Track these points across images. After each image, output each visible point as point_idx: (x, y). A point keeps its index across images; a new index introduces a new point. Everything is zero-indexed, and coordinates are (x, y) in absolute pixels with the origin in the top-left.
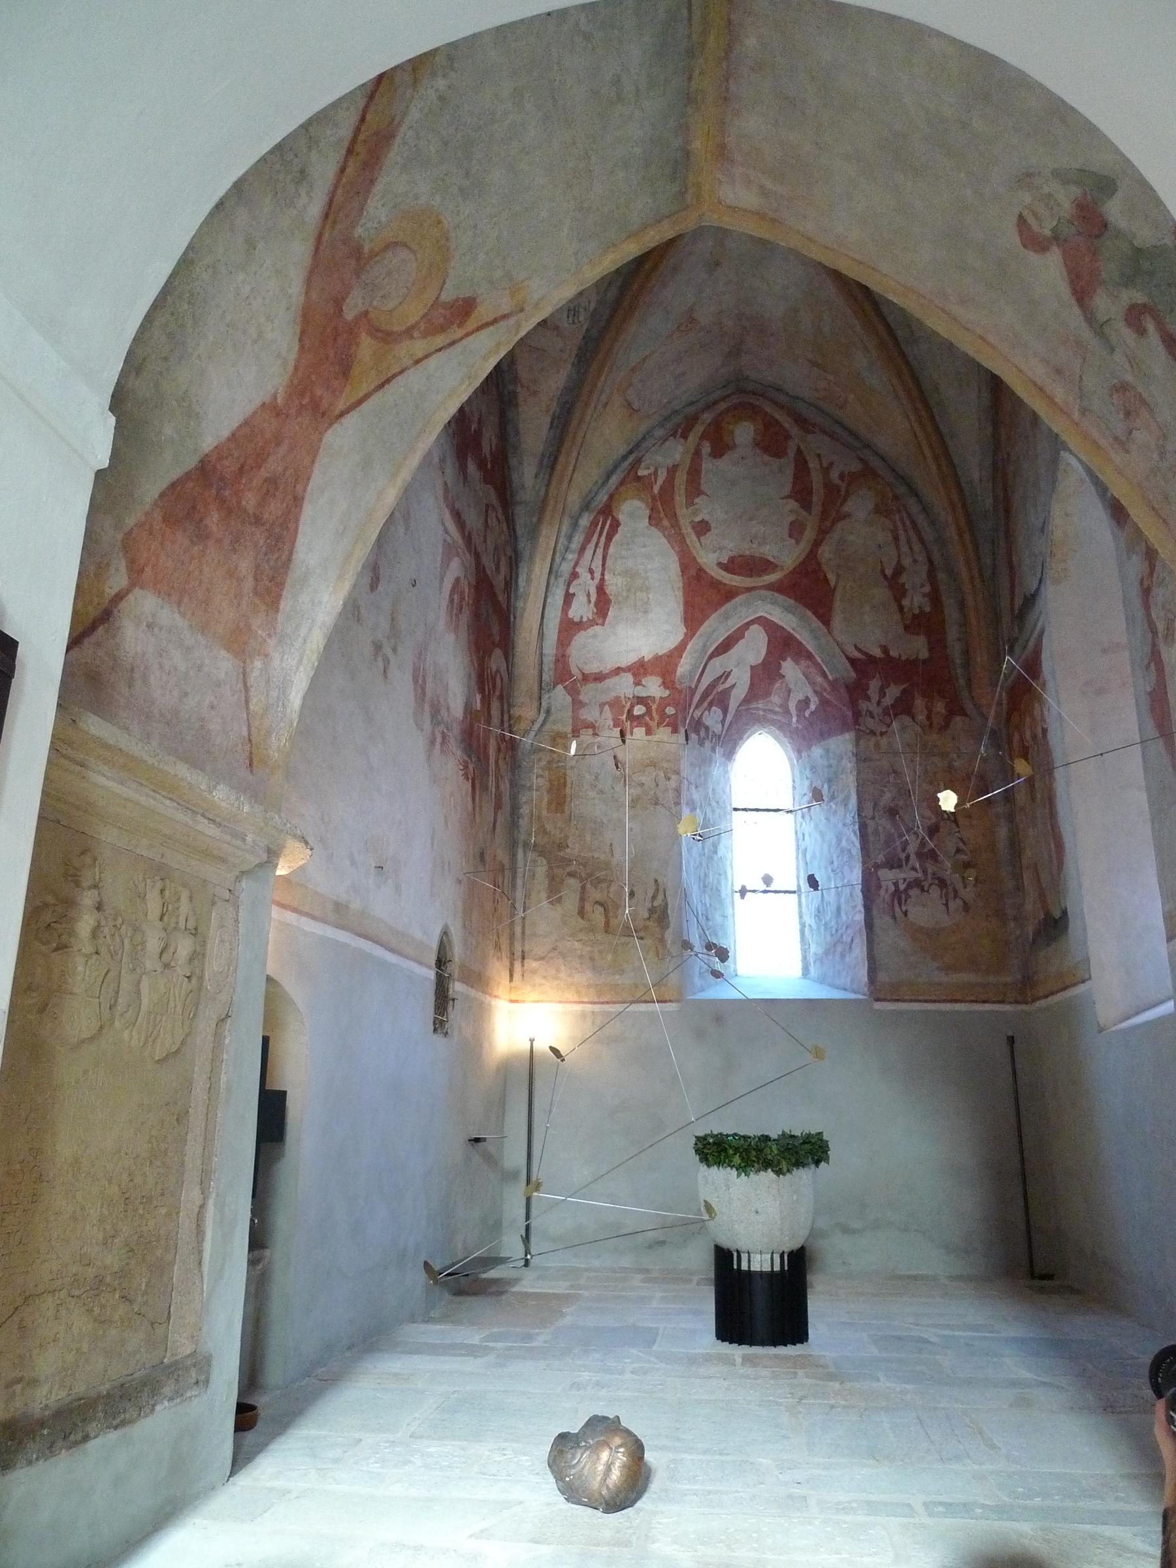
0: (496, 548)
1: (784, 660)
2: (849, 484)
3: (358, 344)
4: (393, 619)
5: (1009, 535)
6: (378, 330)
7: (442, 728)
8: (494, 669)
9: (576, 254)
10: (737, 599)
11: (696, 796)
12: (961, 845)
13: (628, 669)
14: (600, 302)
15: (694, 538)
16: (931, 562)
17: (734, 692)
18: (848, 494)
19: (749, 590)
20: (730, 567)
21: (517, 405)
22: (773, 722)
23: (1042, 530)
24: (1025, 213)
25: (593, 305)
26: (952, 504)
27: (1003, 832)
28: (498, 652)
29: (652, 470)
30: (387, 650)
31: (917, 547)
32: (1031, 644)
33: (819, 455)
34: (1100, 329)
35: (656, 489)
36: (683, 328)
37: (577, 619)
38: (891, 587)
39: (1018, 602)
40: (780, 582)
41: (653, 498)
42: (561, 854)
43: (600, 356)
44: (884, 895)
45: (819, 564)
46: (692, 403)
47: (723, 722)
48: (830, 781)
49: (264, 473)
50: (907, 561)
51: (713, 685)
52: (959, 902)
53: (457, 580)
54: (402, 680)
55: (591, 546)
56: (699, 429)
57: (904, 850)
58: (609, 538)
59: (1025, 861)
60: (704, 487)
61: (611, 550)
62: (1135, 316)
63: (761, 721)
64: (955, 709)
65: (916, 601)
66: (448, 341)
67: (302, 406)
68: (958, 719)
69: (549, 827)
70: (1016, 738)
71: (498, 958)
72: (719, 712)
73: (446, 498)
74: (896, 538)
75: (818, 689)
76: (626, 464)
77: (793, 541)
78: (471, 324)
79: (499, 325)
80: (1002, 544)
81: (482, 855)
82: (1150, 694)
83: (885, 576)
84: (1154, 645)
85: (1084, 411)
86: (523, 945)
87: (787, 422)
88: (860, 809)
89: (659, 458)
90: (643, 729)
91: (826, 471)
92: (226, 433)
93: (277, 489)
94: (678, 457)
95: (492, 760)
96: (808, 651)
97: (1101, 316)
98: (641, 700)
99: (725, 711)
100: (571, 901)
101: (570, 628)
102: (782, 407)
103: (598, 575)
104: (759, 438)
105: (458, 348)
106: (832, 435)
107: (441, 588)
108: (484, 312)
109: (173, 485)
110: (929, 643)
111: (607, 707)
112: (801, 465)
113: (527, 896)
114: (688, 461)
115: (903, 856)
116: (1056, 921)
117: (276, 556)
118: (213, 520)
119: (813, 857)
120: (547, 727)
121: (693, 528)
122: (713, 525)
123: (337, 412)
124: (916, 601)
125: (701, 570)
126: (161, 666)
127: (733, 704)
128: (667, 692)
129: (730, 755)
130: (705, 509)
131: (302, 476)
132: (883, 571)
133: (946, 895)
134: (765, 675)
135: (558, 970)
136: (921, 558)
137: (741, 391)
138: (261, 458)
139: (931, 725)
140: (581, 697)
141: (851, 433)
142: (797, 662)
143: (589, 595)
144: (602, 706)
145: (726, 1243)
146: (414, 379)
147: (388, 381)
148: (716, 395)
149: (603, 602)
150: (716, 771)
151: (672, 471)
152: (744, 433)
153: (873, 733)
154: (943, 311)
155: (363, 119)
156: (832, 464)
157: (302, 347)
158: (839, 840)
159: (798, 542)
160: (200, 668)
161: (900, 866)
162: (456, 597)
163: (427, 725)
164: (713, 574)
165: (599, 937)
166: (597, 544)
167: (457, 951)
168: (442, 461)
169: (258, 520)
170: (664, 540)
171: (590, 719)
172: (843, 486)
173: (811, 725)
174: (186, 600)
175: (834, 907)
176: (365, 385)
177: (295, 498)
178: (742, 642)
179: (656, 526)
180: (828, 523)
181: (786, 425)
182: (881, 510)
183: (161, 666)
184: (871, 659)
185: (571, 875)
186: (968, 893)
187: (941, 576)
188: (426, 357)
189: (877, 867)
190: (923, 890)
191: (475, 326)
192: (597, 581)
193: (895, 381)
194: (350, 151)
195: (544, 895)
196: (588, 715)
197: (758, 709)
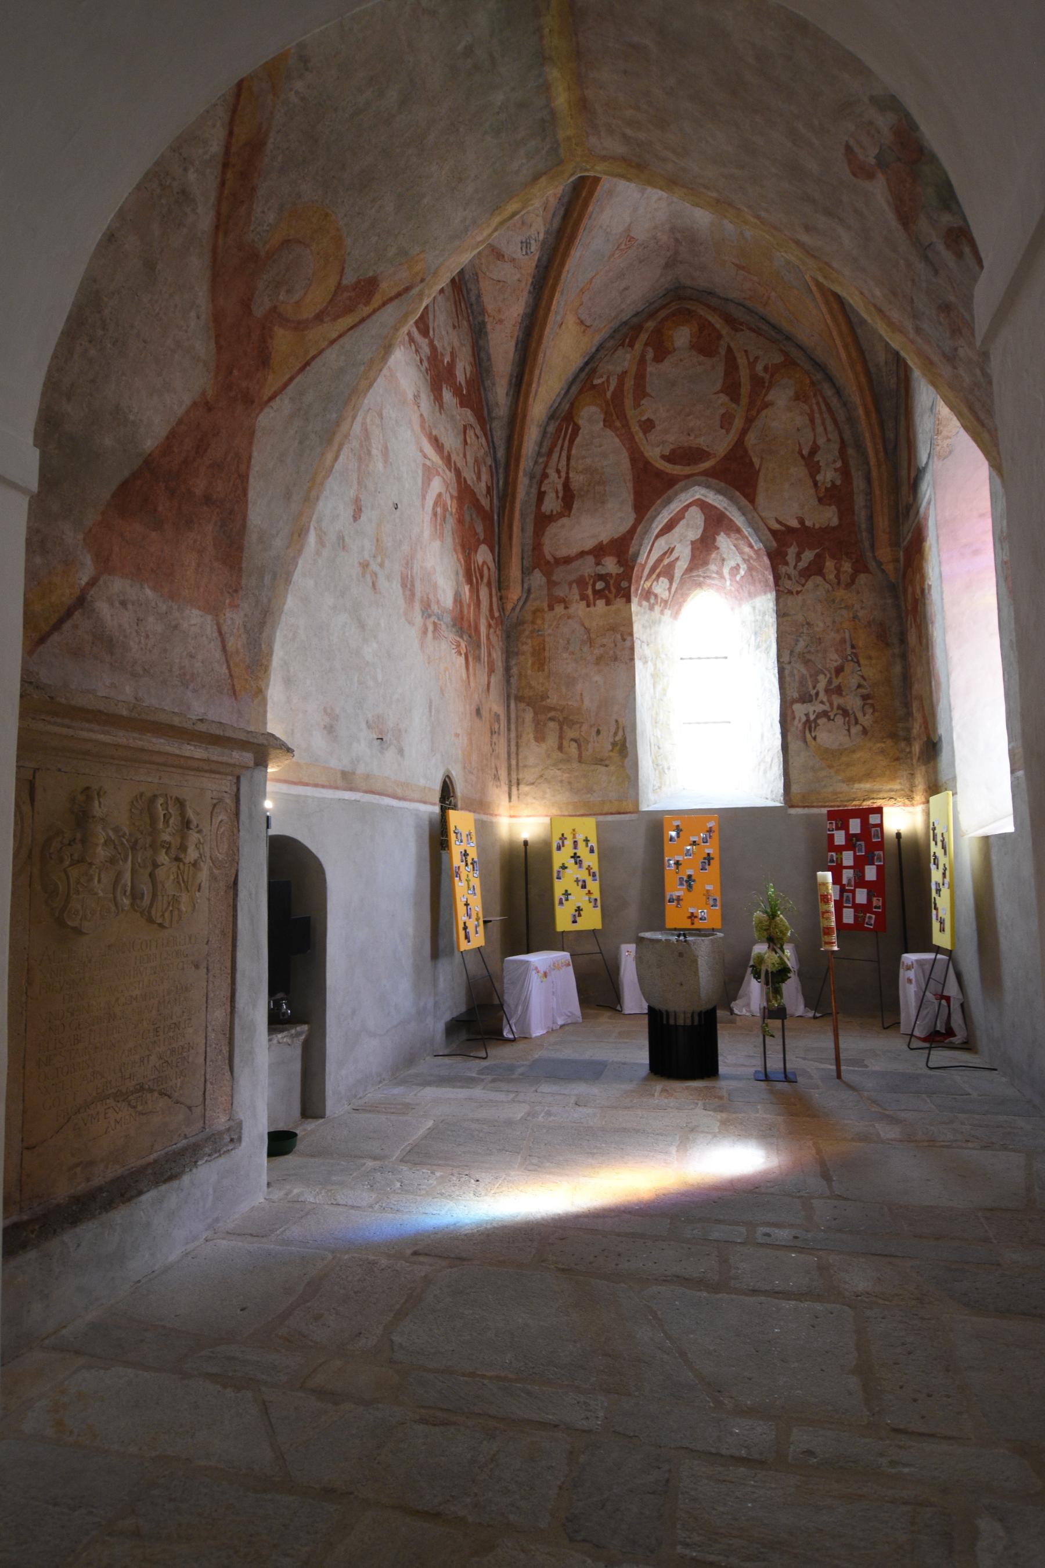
0: (476, 461)
1: (718, 534)
2: (772, 376)
4: (378, 540)
7: (433, 619)
8: (480, 563)
10: (677, 487)
12: (863, 682)
13: (590, 552)
14: (547, 232)
15: (641, 434)
17: (679, 563)
19: (688, 477)
20: (671, 458)
21: (486, 334)
24: (852, 143)
25: (541, 237)
27: (898, 669)
28: (483, 549)
29: (605, 377)
30: (374, 567)
31: (830, 427)
33: (746, 351)
34: (924, 251)
35: (609, 395)
36: (623, 247)
37: (548, 513)
38: (807, 465)
40: (713, 467)
42: (544, 703)
43: (551, 282)
44: (797, 724)
45: (746, 452)
46: (637, 314)
47: (670, 589)
50: (821, 441)
51: (660, 560)
52: (859, 728)
53: (440, 495)
54: (392, 589)
55: (557, 449)
56: (644, 337)
57: (814, 688)
58: (572, 442)
60: (648, 390)
61: (573, 452)
64: (860, 567)
65: (828, 476)
66: (357, 320)
69: (533, 683)
71: (497, 787)
72: (666, 581)
73: (423, 427)
74: (812, 420)
75: (746, 557)
76: (583, 375)
77: (724, 431)
80: (902, 418)
83: (802, 456)
86: (518, 774)
87: (718, 323)
89: (610, 367)
90: (604, 601)
91: (752, 365)
94: (626, 364)
96: (736, 526)
98: (601, 577)
99: (671, 581)
100: (552, 741)
101: (543, 521)
102: (714, 309)
103: (563, 474)
104: (695, 340)
106: (757, 331)
107: (423, 506)
108: (386, 287)
111: (574, 585)
113: (518, 737)
115: (813, 692)
120: (529, 603)
121: (640, 426)
122: (657, 422)
123: (265, 398)
125: (647, 463)
127: (678, 573)
128: (622, 569)
130: (650, 409)
133: (848, 722)
135: (545, 793)
136: (834, 436)
139: (839, 583)
140: (554, 578)
141: (774, 327)
143: (557, 492)
152: (682, 336)
153: (790, 592)
155: (231, 133)
156: (757, 358)
159: (728, 431)
161: (811, 701)
162: (439, 510)
163: (418, 619)
164: (657, 465)
165: (575, 765)
166: (562, 447)
168: (416, 397)
169: (207, 500)
170: (616, 440)
171: (562, 595)
173: (741, 586)
178: (683, 523)
179: (610, 427)
180: (754, 413)
181: (718, 326)
182: (800, 397)
184: (790, 530)
185: (552, 719)
186: (866, 720)
187: (851, 451)
189: (794, 701)
190: (829, 719)
191: (380, 302)
192: (563, 479)
194: (225, 165)
195: (531, 736)
196: (560, 592)
197: (699, 576)
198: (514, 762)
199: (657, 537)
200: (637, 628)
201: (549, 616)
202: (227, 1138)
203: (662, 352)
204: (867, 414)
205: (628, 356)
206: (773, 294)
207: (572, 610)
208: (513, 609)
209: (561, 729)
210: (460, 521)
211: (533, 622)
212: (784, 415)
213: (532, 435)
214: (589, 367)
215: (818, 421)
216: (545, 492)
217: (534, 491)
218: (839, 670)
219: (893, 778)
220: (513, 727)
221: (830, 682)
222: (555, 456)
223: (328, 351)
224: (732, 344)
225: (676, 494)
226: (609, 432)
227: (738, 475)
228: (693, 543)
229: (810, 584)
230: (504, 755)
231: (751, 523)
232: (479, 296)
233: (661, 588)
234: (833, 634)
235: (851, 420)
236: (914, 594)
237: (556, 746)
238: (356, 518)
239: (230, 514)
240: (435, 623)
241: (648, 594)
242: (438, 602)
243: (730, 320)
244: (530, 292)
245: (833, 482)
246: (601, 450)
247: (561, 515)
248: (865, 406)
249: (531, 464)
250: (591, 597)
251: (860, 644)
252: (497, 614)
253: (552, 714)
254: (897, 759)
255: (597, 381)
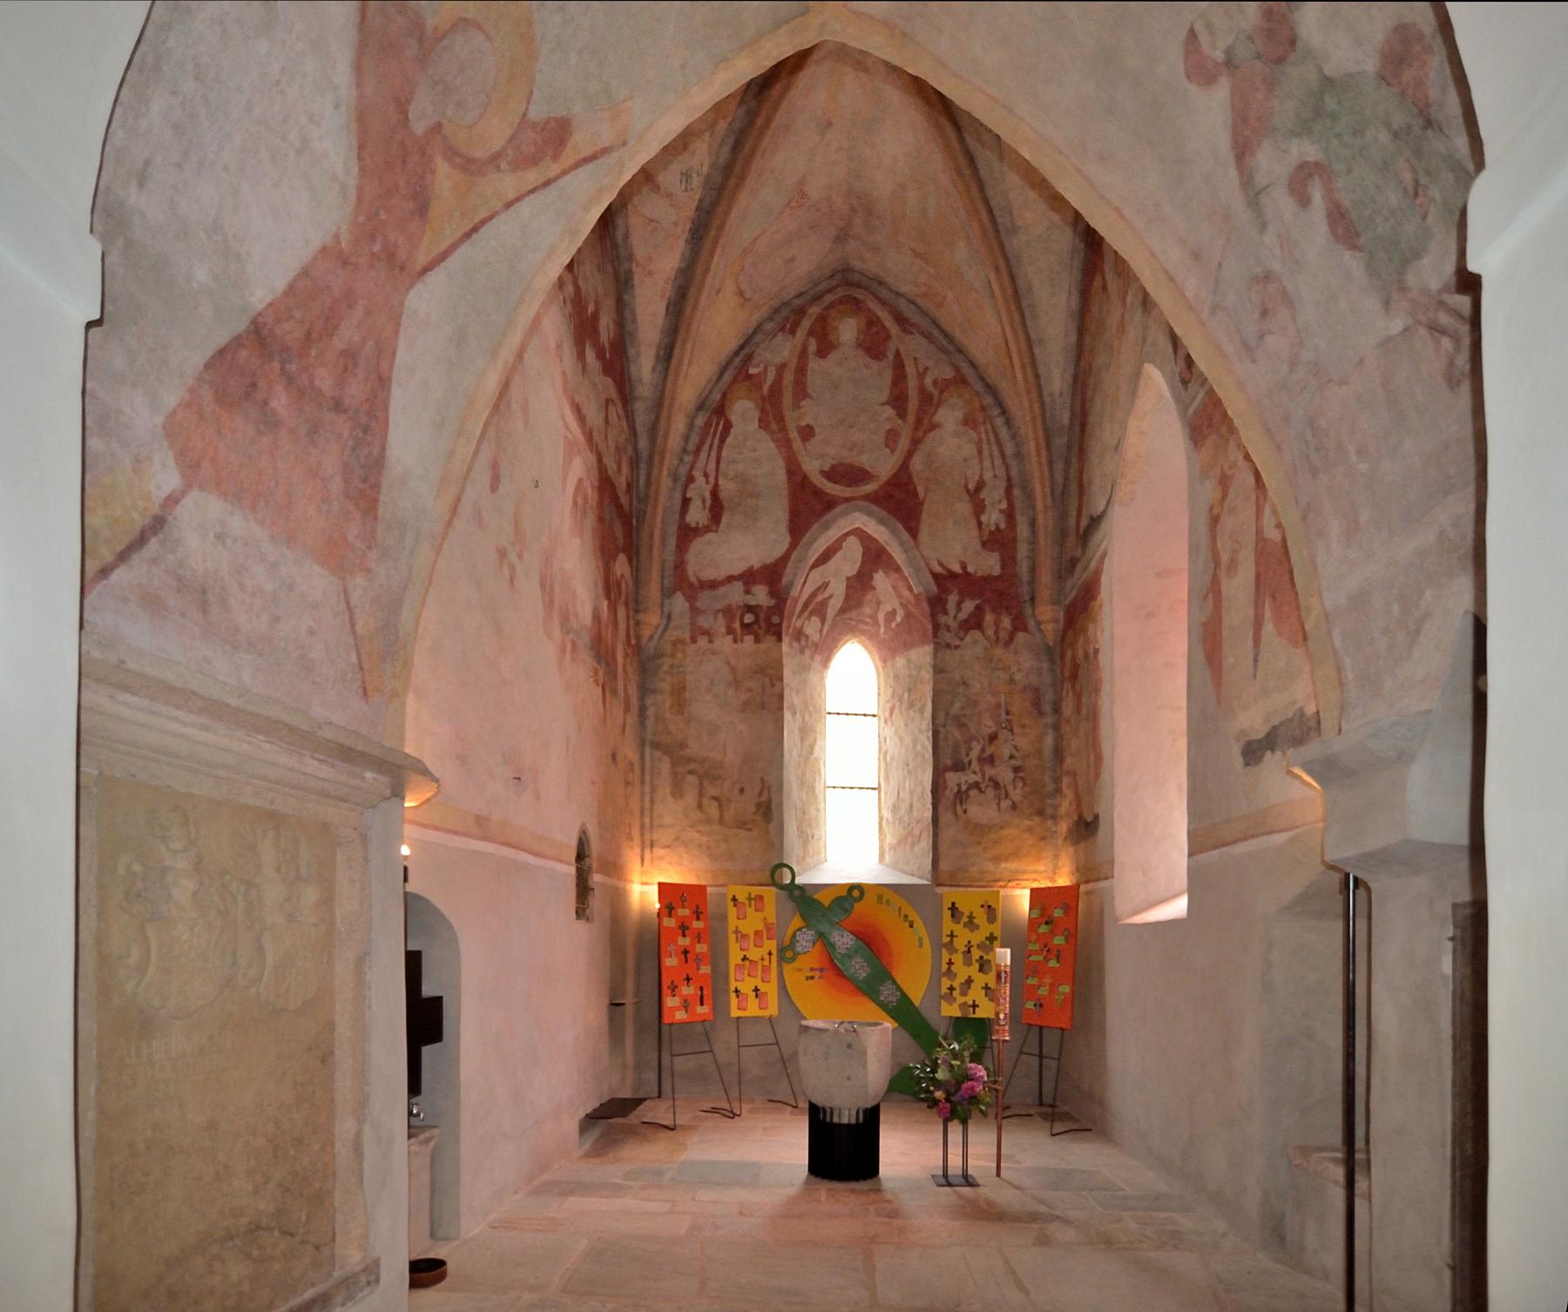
2: (942, 392)
3: (433, 172)
5: (1082, 452)
6: (456, 153)
7: (572, 636)
9: (683, 67)
11: (797, 701)
14: (713, 166)
16: (1009, 479)
17: (832, 601)
18: (940, 402)
19: (847, 500)
20: (832, 475)
22: (863, 633)
23: (1116, 448)
25: (705, 169)
26: (1033, 419)
27: (1049, 741)
28: (622, 558)
30: (513, 556)
31: (998, 462)
32: (1093, 565)
34: (1254, 196)
39: (1084, 522)
40: (875, 492)
41: (763, 399)
43: (713, 233)
45: (910, 475)
46: (801, 295)
48: (909, 690)
49: (339, 343)
50: (988, 476)
51: (813, 595)
53: (580, 481)
54: (529, 587)
55: (706, 447)
56: (806, 324)
59: (1065, 767)
60: (809, 390)
61: (724, 453)
62: (1300, 181)
63: (853, 630)
64: (1019, 625)
65: (993, 517)
66: (542, 180)
67: (373, 254)
68: (1021, 634)
69: (672, 728)
70: (1069, 654)
73: (565, 390)
74: (980, 451)
76: (737, 360)
78: (569, 156)
79: (599, 162)
81: (614, 758)
82: (1204, 624)
84: (1215, 576)
85: (1214, 309)
87: (889, 322)
88: (934, 717)
89: (768, 355)
91: (921, 376)
92: (280, 285)
93: (356, 365)
94: (786, 353)
95: (620, 668)
97: (1261, 180)
98: (750, 609)
99: (823, 621)
100: (690, 798)
101: (687, 534)
102: (884, 303)
103: (712, 480)
105: (552, 191)
106: (929, 337)
107: (563, 490)
108: (581, 142)
109: (221, 352)
110: (1003, 560)
112: (899, 366)
113: (653, 791)
114: (795, 360)
116: (1087, 824)
117: (366, 451)
118: (280, 401)
119: (892, 758)
122: (817, 430)
123: (419, 268)
124: (993, 517)
125: (805, 477)
126: (241, 586)
127: (831, 612)
128: (772, 602)
129: (826, 663)
131: (385, 351)
132: (966, 486)
134: (860, 584)
136: (1001, 472)
137: (848, 284)
138: (331, 322)
140: (698, 604)
141: (946, 335)
142: (886, 574)
144: (717, 612)
145: (819, 1101)
146: (503, 230)
147: (475, 229)
148: (821, 287)
149: (716, 509)
150: (813, 678)
151: (781, 368)
152: (848, 330)
153: (948, 646)
154: (1078, 170)
156: (927, 369)
157: (362, 169)
158: (915, 743)
159: (893, 451)
160: (291, 587)
161: (963, 770)
165: (715, 827)
167: (595, 847)
168: (559, 347)
170: (772, 445)
171: (706, 626)
172: (936, 392)
174: (262, 504)
175: (907, 804)
176: (448, 232)
177: (380, 379)
178: (840, 553)
180: (920, 433)
181: (887, 324)
182: (969, 421)
183: (241, 586)
184: (952, 575)
185: (690, 772)
186: (1016, 794)
187: (1016, 492)
188: (518, 199)
189: (947, 769)
192: (710, 486)
193: (992, 276)
195: (668, 791)
196: (704, 622)
198: (647, 821)
199: (814, 566)
200: (787, 672)
201: (691, 648)
202: (363, 1279)
203: (826, 346)
204: (1038, 451)
205: (789, 345)
206: (950, 294)
207: (717, 642)
208: (651, 637)
209: (701, 786)
210: (601, 519)
211: (673, 656)
212: (951, 443)
213: (678, 426)
214: (744, 352)
215: (986, 453)
216: (690, 499)
217: (678, 496)
218: (993, 738)
219: (1038, 859)
220: (647, 778)
221: (983, 750)
222: (703, 455)
223: (503, 216)
224: (902, 349)
225: (835, 519)
226: (763, 434)
227: (901, 501)
228: (848, 579)
229: (968, 639)
230: (637, 813)
231: (911, 561)
232: (627, 236)
233: (812, 628)
234: (989, 697)
235: (1019, 455)
236: (1074, 658)
237: (695, 804)
238: (494, 488)
239: (365, 432)
240: (573, 643)
241: (799, 635)
242: (576, 616)
243: (900, 319)
244: (687, 242)
245: (997, 526)
246: (753, 456)
247: (707, 529)
248: (1036, 439)
249: (676, 462)
250: (739, 630)
251: (1015, 709)
252: (633, 642)
253: (692, 766)
254: (1043, 839)
255: (753, 371)
